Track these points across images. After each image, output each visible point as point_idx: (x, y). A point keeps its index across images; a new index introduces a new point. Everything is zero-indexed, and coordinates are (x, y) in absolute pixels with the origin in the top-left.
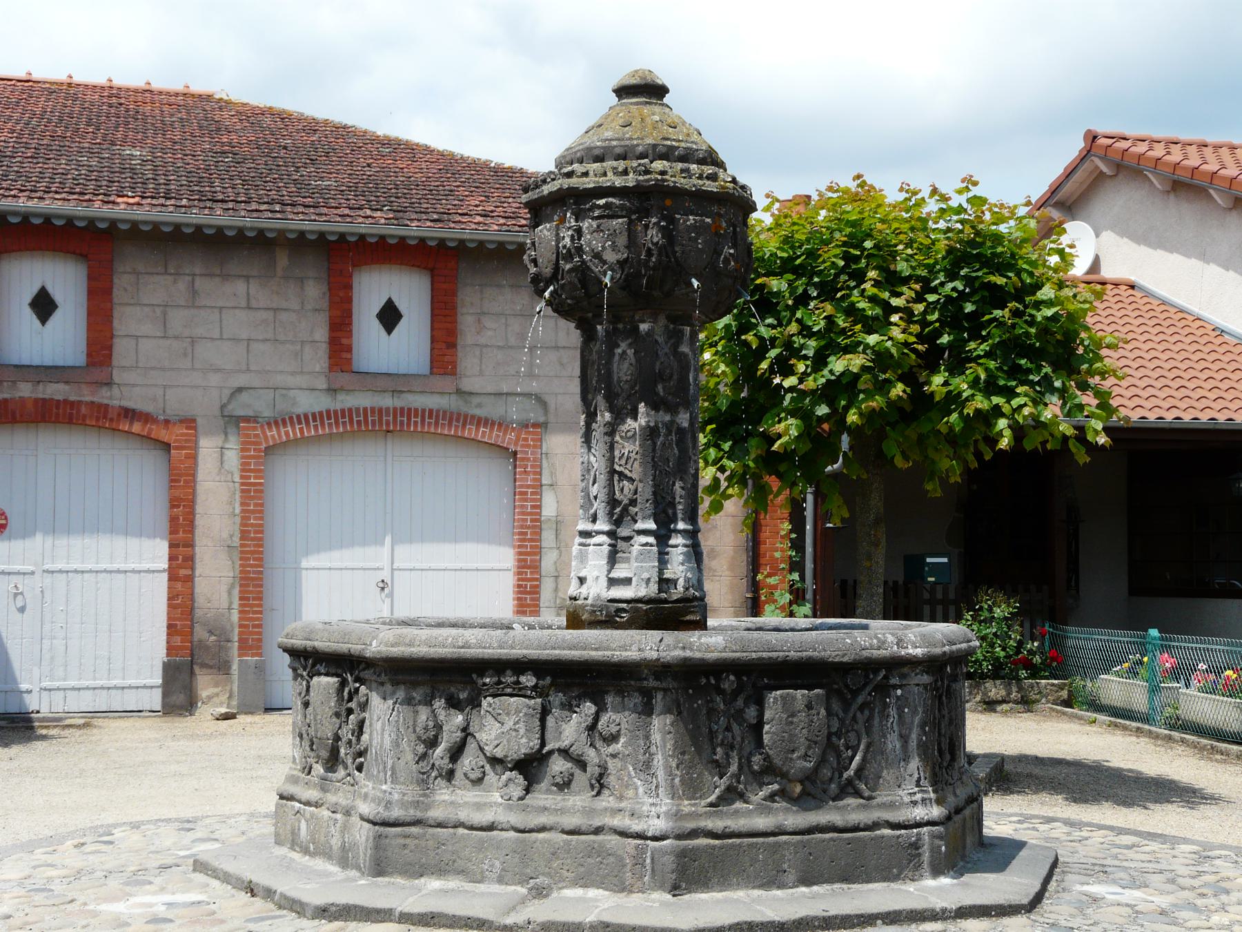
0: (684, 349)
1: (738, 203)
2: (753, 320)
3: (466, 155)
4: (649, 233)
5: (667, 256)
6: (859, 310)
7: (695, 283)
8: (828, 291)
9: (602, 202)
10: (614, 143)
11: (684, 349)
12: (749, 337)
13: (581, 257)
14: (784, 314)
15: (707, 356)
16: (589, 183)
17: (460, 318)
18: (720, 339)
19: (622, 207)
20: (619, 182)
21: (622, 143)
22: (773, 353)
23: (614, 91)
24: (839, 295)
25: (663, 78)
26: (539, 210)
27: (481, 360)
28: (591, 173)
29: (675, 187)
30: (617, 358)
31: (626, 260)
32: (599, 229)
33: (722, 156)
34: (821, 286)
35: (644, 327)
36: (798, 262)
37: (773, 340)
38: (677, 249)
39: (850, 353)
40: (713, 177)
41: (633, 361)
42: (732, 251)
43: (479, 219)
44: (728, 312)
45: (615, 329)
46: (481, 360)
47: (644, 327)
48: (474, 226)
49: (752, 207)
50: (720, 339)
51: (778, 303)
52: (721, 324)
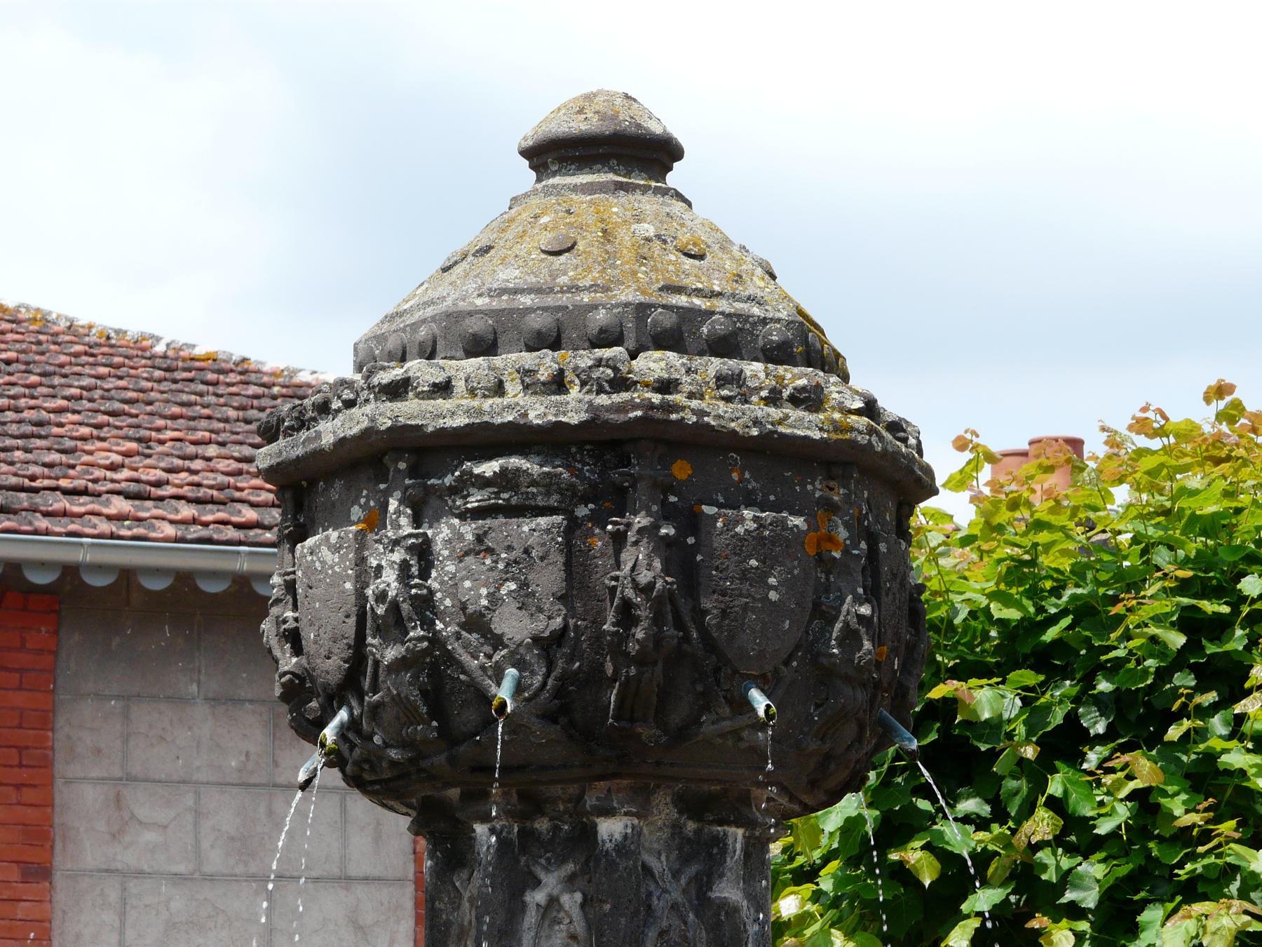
0: (729, 891)
1: (884, 473)
2: (924, 805)
3: (83, 319)
4: (628, 557)
5: (679, 624)
6: (1228, 773)
7: (760, 701)
8: (1140, 720)
9: (489, 468)
10: (526, 300)
11: (729, 891)
12: (914, 855)
13: (428, 624)
14: (1010, 784)
15: (789, 905)
16: (453, 414)
17: (62, 793)
18: (826, 860)
19: (548, 483)
20: (539, 411)
21: (550, 301)
22: (984, 899)
23: (527, 153)
24: (1174, 733)
25: (665, 114)
26: (305, 493)
27: (122, 915)
28: (459, 386)
29: (701, 427)
30: (531, 918)
31: (559, 637)
32: (481, 546)
33: (836, 338)
34: (1116, 705)
35: (611, 829)
36: (1051, 634)
37: (983, 858)
38: (707, 603)
39: (1204, 897)
40: (810, 399)
41: (579, 927)
42: (865, 610)
43: (120, 505)
44: (855, 783)
45: (526, 834)
46: (122, 915)
47: (611, 829)
48: (104, 527)
49: (919, 484)
50: (826, 860)
51: (993, 755)
52: (833, 819)
